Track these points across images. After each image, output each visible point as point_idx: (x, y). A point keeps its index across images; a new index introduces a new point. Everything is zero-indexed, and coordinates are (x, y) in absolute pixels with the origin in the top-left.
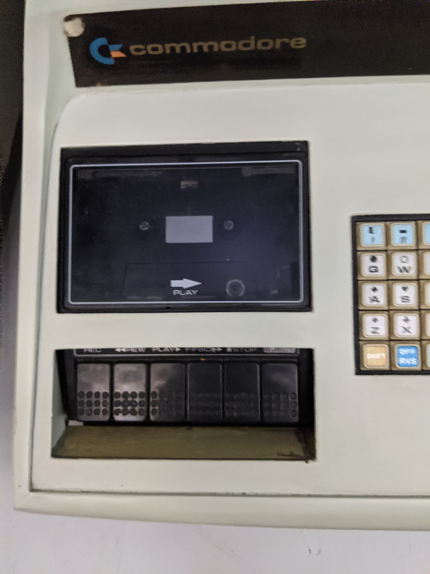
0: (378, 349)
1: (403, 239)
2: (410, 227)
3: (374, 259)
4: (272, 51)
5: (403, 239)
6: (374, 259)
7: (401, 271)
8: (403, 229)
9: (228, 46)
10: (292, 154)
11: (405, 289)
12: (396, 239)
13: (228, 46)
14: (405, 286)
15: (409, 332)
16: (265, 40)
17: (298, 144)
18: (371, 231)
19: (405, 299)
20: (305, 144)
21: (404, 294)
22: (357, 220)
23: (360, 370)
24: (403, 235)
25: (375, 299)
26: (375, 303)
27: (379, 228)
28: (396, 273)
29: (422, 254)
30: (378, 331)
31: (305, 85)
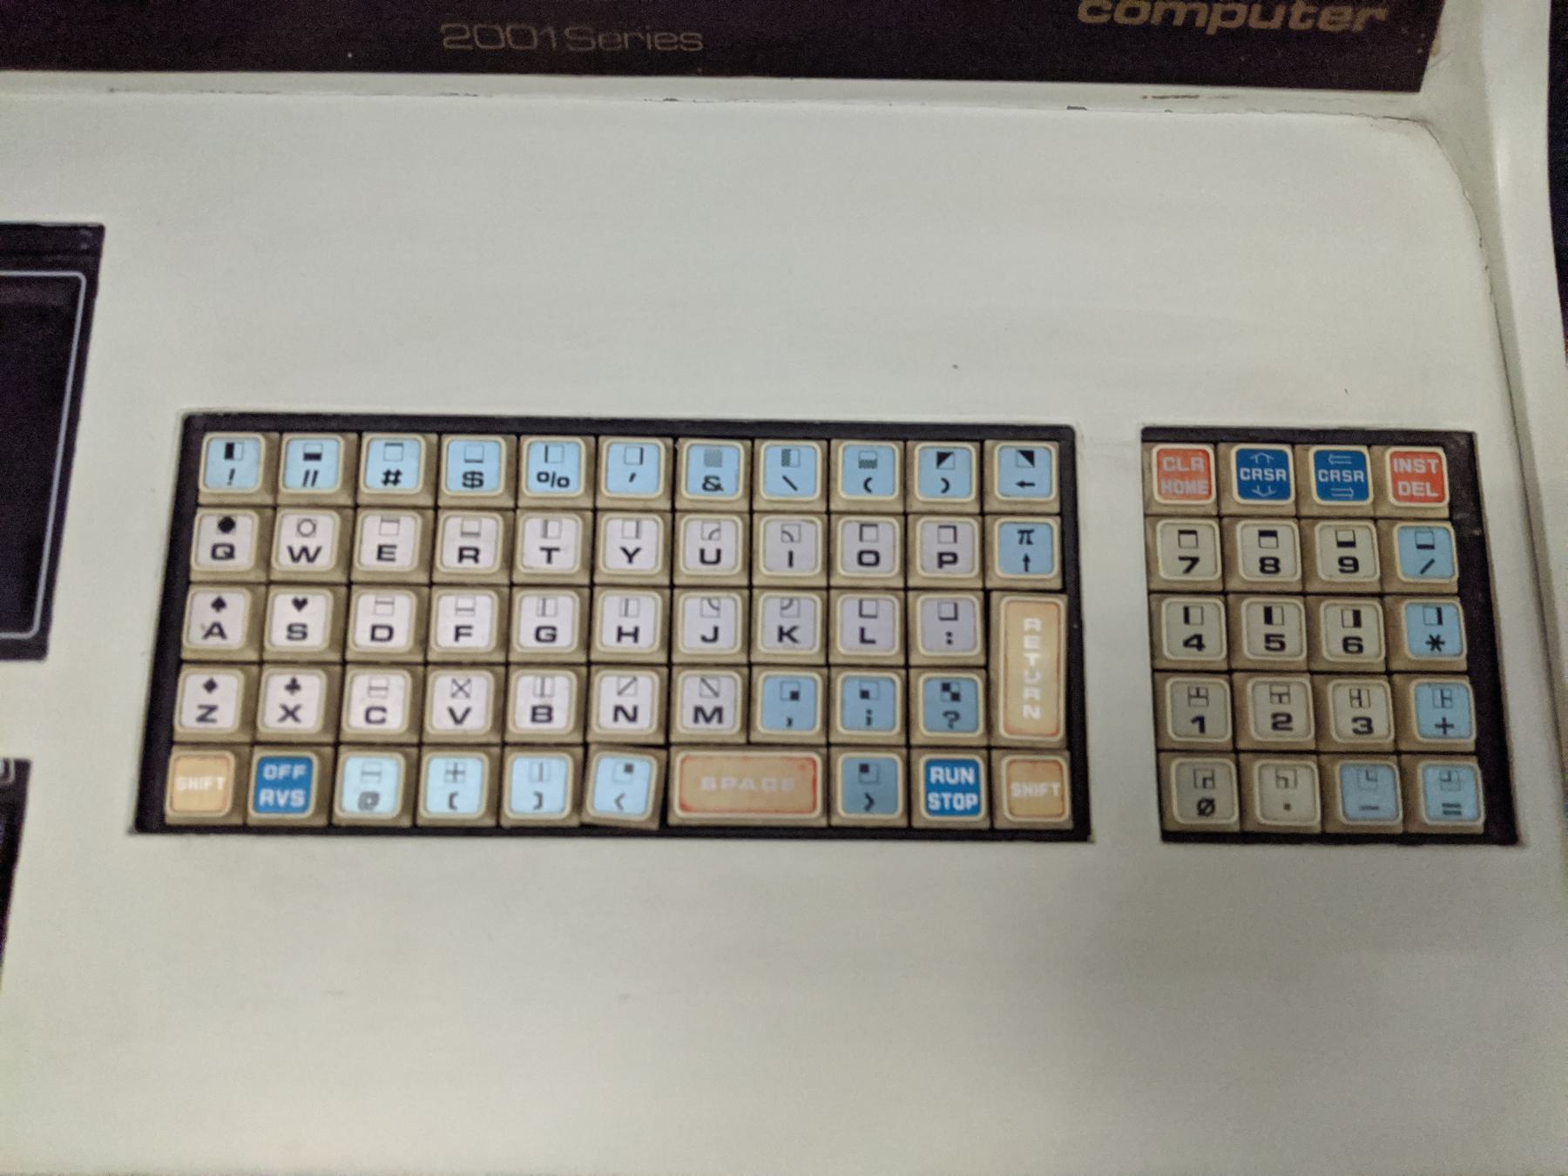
0: (209, 763)
1: (311, 477)
2: (332, 447)
3: (227, 525)
4: (1147, 27)
5: (311, 477)
6: (227, 525)
7: (295, 559)
8: (313, 449)
9: (1229, 16)
10: (67, 258)
11: (300, 604)
12: (614, 484)
13: (1229, 16)
14: (300, 598)
15: (296, 720)
16: (1230, 7)
17: (87, 233)
18: (230, 452)
19: (297, 631)
20: (99, 231)
21: (296, 617)
22: (194, 429)
23: (668, 826)
24: (312, 465)
25: (217, 630)
26: (214, 641)
27: (252, 447)
28: (283, 563)
29: (1233, 525)
30: (213, 715)
31: (135, 89)
